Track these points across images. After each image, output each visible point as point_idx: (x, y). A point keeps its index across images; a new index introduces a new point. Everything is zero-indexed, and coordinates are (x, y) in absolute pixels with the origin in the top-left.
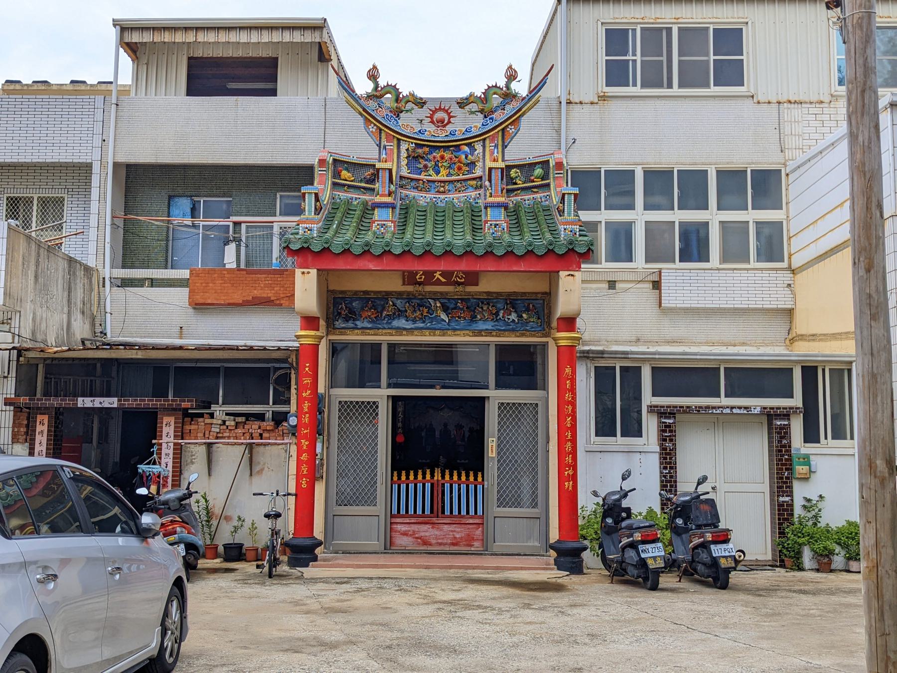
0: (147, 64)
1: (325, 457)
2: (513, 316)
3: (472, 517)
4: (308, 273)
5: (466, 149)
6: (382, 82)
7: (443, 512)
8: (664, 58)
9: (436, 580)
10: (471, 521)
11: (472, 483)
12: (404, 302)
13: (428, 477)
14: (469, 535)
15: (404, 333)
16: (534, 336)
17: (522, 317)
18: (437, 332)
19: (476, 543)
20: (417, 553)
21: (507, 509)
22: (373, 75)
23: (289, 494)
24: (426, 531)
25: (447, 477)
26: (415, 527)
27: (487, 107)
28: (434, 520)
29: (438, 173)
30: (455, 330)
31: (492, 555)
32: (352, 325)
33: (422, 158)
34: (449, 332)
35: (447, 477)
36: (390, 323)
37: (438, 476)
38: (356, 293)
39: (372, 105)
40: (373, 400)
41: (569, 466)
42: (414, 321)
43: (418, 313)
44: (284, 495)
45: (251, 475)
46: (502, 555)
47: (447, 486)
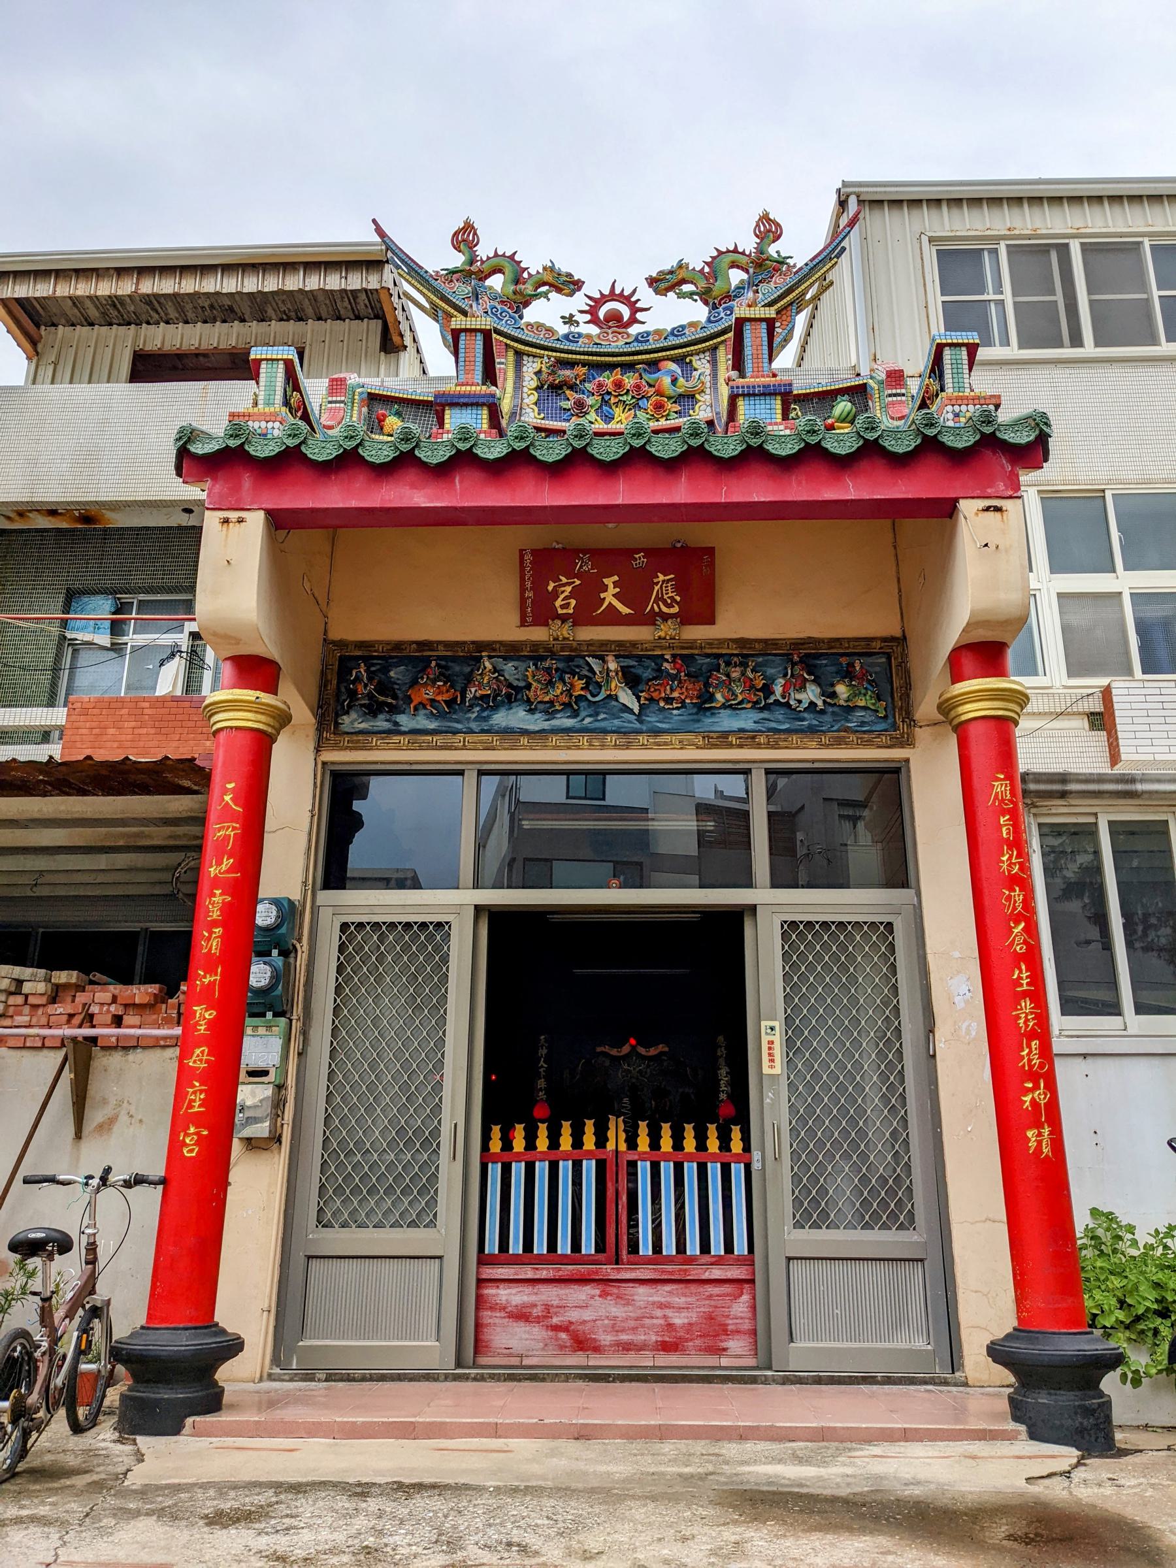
0: (56, 364)
1: (291, 1081)
2: (812, 694)
3: (718, 1261)
4: (241, 521)
5: (673, 366)
6: (484, 251)
7: (634, 1247)
8: (1059, 297)
9: (609, 1495)
10: (717, 1273)
11: (714, 1158)
12: (522, 666)
13: (589, 1142)
14: (710, 1318)
15: (524, 740)
16: (868, 744)
17: (834, 695)
18: (611, 739)
19: (736, 1343)
20: (555, 1378)
21: (823, 1234)
22: (465, 237)
23: (139, 1180)
24: (583, 1305)
25: (643, 1143)
26: (551, 1294)
27: (718, 287)
28: (609, 1271)
29: (608, 418)
30: (657, 732)
31: (785, 1381)
32: (386, 725)
33: (572, 387)
34: (643, 739)
35: (643, 1143)
36: (486, 719)
37: (616, 1139)
38: (398, 646)
39: (460, 291)
40: (436, 919)
41: (1034, 1076)
42: (549, 710)
43: (560, 688)
44: (128, 1184)
45: (78, 1135)
46: (818, 1381)
47: (644, 1169)
